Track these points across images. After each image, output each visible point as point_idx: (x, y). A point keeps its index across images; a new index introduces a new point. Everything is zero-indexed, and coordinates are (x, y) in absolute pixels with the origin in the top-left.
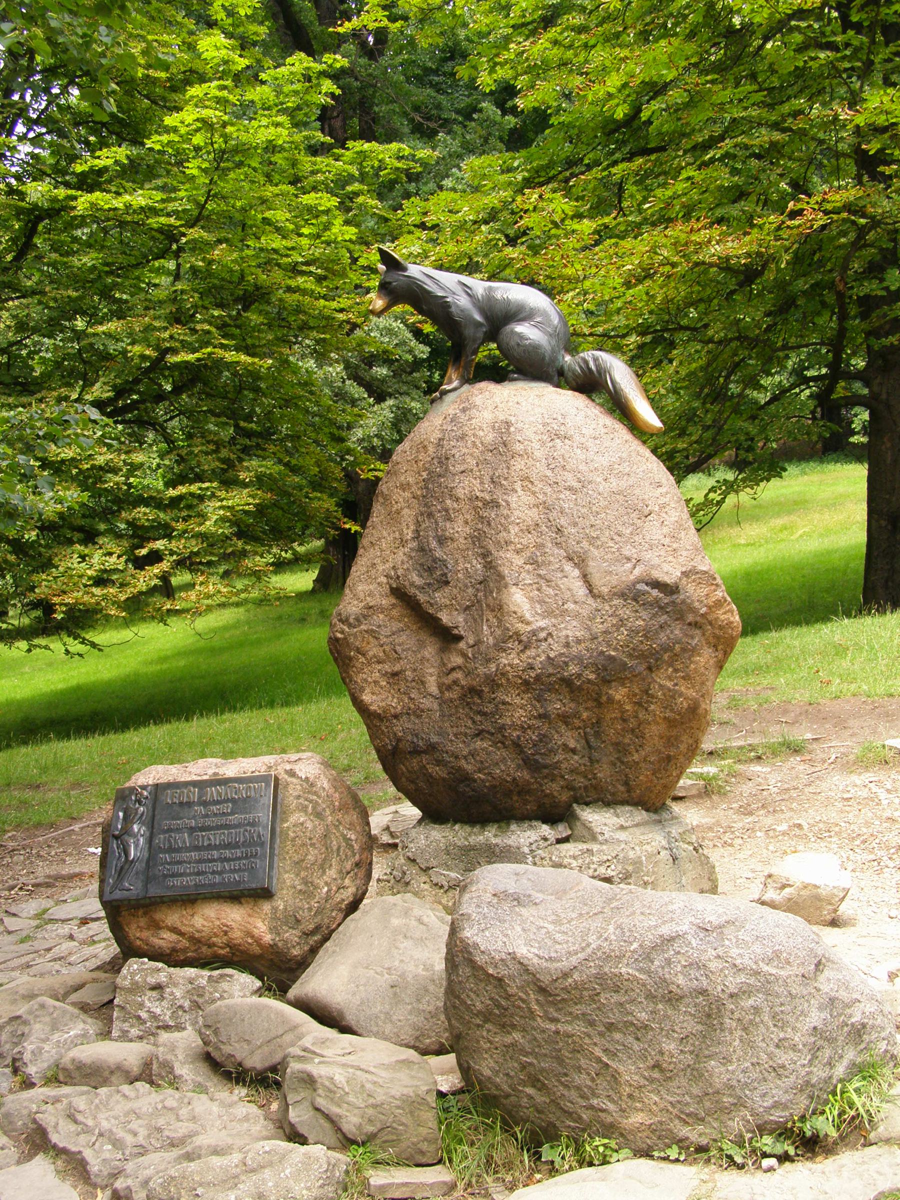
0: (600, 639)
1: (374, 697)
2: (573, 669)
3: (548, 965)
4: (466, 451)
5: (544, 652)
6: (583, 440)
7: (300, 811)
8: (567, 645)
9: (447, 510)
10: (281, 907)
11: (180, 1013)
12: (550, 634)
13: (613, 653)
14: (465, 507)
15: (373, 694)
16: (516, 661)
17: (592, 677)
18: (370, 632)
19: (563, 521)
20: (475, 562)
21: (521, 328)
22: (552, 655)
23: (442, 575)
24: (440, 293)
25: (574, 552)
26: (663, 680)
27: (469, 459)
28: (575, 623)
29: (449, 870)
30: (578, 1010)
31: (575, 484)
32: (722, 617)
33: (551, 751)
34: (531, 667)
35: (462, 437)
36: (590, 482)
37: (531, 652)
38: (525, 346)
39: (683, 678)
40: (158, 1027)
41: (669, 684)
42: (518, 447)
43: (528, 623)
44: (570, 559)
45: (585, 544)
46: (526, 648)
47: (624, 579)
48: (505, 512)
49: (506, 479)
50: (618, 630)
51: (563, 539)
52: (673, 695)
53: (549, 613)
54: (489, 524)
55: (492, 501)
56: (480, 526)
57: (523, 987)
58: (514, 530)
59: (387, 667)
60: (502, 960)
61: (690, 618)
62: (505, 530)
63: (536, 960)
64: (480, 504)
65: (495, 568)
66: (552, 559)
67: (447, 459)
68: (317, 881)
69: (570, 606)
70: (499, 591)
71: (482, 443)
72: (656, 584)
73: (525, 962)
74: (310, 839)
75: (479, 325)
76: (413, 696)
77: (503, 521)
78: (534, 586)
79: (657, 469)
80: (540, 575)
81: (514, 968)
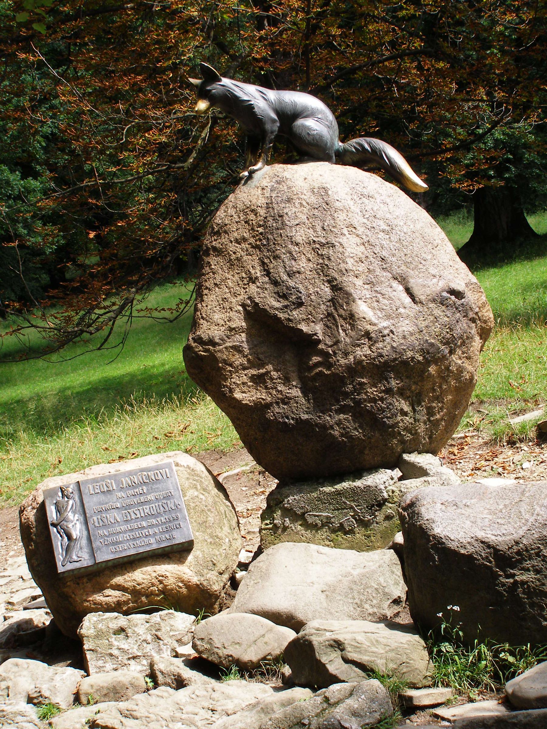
0: (424, 332)
1: (244, 395)
2: (410, 354)
3: (503, 538)
4: (297, 210)
5: (388, 343)
6: (382, 198)
7: (192, 488)
8: (404, 337)
9: (290, 253)
10: (201, 556)
11: (145, 645)
12: (392, 331)
13: (433, 341)
14: (307, 249)
15: (243, 392)
16: (369, 352)
17: (421, 358)
18: (233, 347)
19: (384, 253)
20: (323, 287)
21: (310, 123)
22: (395, 345)
23: (297, 298)
24: (245, 98)
25: (397, 273)
26: (456, 360)
27: (300, 215)
28: (407, 322)
29: (320, 512)
30: (528, 564)
31: (387, 228)
32: (485, 314)
33: (392, 415)
34: (381, 356)
35: (289, 200)
36: (396, 226)
37: (380, 345)
38: (313, 135)
39: (467, 357)
40: (129, 659)
41: (459, 362)
42: (337, 204)
43: (375, 325)
44: (396, 279)
45: (403, 267)
46: (375, 342)
47: (434, 289)
48: (341, 250)
49: (334, 227)
50: (434, 325)
51: (388, 265)
52: (460, 370)
53: (388, 317)
54: (329, 259)
55: (328, 243)
56: (321, 261)
57: (487, 557)
58: (350, 261)
59: (254, 372)
60: (469, 543)
61: (471, 315)
62: (344, 262)
63: (493, 538)
64: (318, 246)
65: (341, 289)
66: (383, 279)
67: (281, 216)
68: (220, 535)
69: (402, 310)
70: (348, 303)
71: (308, 203)
72: (452, 292)
73: (486, 540)
74: (206, 506)
75: (274, 121)
76: (279, 389)
77: (340, 256)
78: (374, 299)
79: (422, 216)
80: (376, 291)
81: (478, 547)
